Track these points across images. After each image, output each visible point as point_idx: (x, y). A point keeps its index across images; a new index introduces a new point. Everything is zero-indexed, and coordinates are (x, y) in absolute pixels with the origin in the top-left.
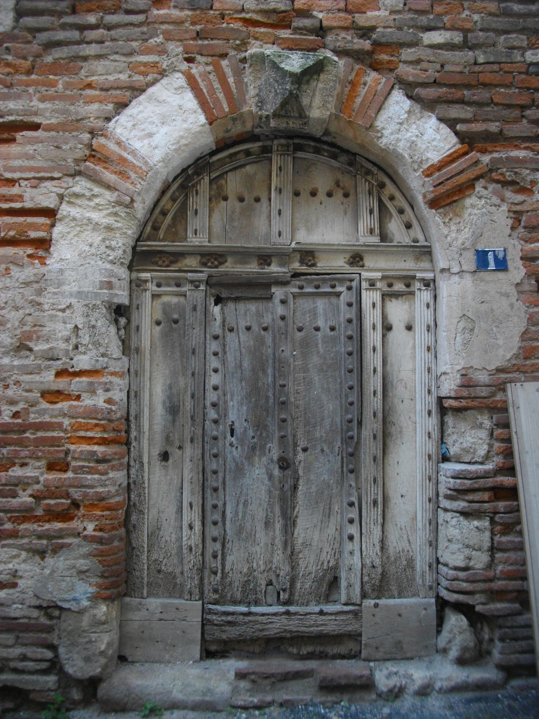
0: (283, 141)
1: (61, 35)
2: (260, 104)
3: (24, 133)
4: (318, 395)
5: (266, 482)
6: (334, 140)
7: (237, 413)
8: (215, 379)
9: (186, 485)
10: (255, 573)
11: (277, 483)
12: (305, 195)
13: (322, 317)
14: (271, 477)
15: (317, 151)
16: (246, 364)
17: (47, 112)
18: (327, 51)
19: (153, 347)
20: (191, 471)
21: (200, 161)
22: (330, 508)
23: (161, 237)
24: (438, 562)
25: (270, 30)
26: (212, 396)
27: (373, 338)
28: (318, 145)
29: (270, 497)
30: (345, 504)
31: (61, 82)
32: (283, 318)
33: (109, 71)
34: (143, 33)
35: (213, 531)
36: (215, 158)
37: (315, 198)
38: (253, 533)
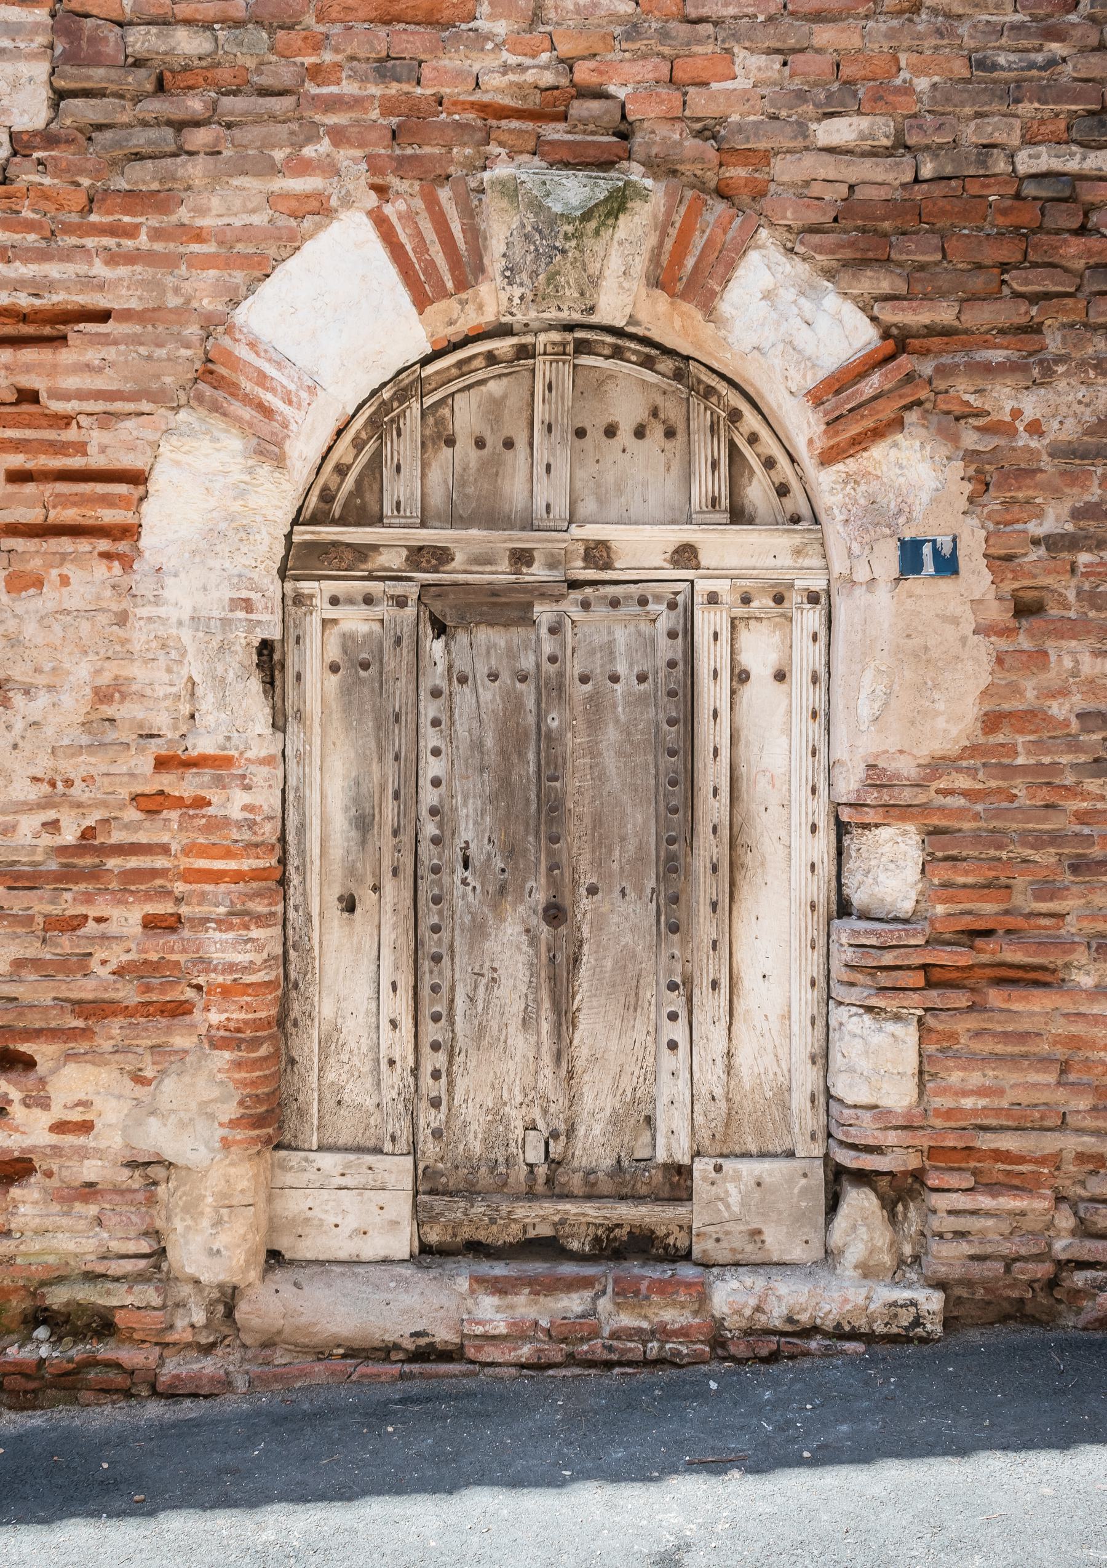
0: (555, 336)
1: (140, 139)
2: (508, 273)
3: (81, 326)
4: (607, 773)
5: (525, 948)
6: (647, 334)
7: (472, 828)
8: (433, 767)
9: (386, 952)
10: (507, 1109)
11: (543, 949)
12: (595, 435)
13: (623, 657)
14: (534, 942)
15: (617, 353)
16: (489, 742)
17: (122, 288)
18: (634, 164)
19: (327, 711)
20: (395, 927)
21: (404, 375)
22: (637, 994)
23: (337, 516)
24: (829, 1096)
25: (529, 125)
26: (430, 796)
27: (712, 694)
28: (619, 342)
29: (532, 976)
30: (663, 987)
31: (144, 230)
32: (553, 659)
33: (226, 204)
34: (293, 133)
35: (432, 1032)
36: (430, 369)
37: (612, 441)
38: (502, 1038)
